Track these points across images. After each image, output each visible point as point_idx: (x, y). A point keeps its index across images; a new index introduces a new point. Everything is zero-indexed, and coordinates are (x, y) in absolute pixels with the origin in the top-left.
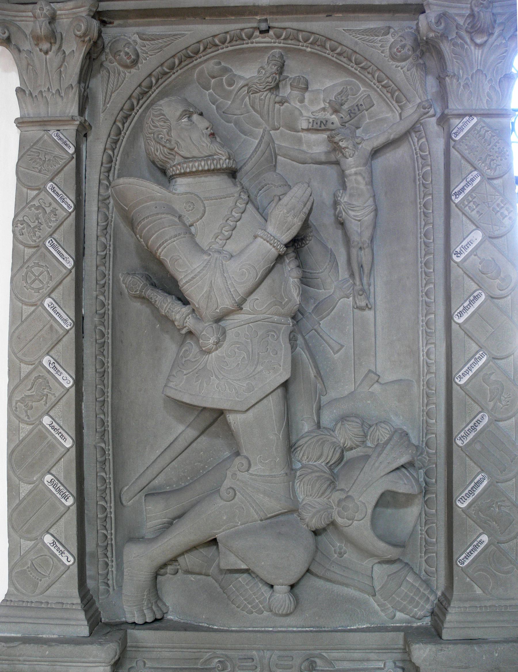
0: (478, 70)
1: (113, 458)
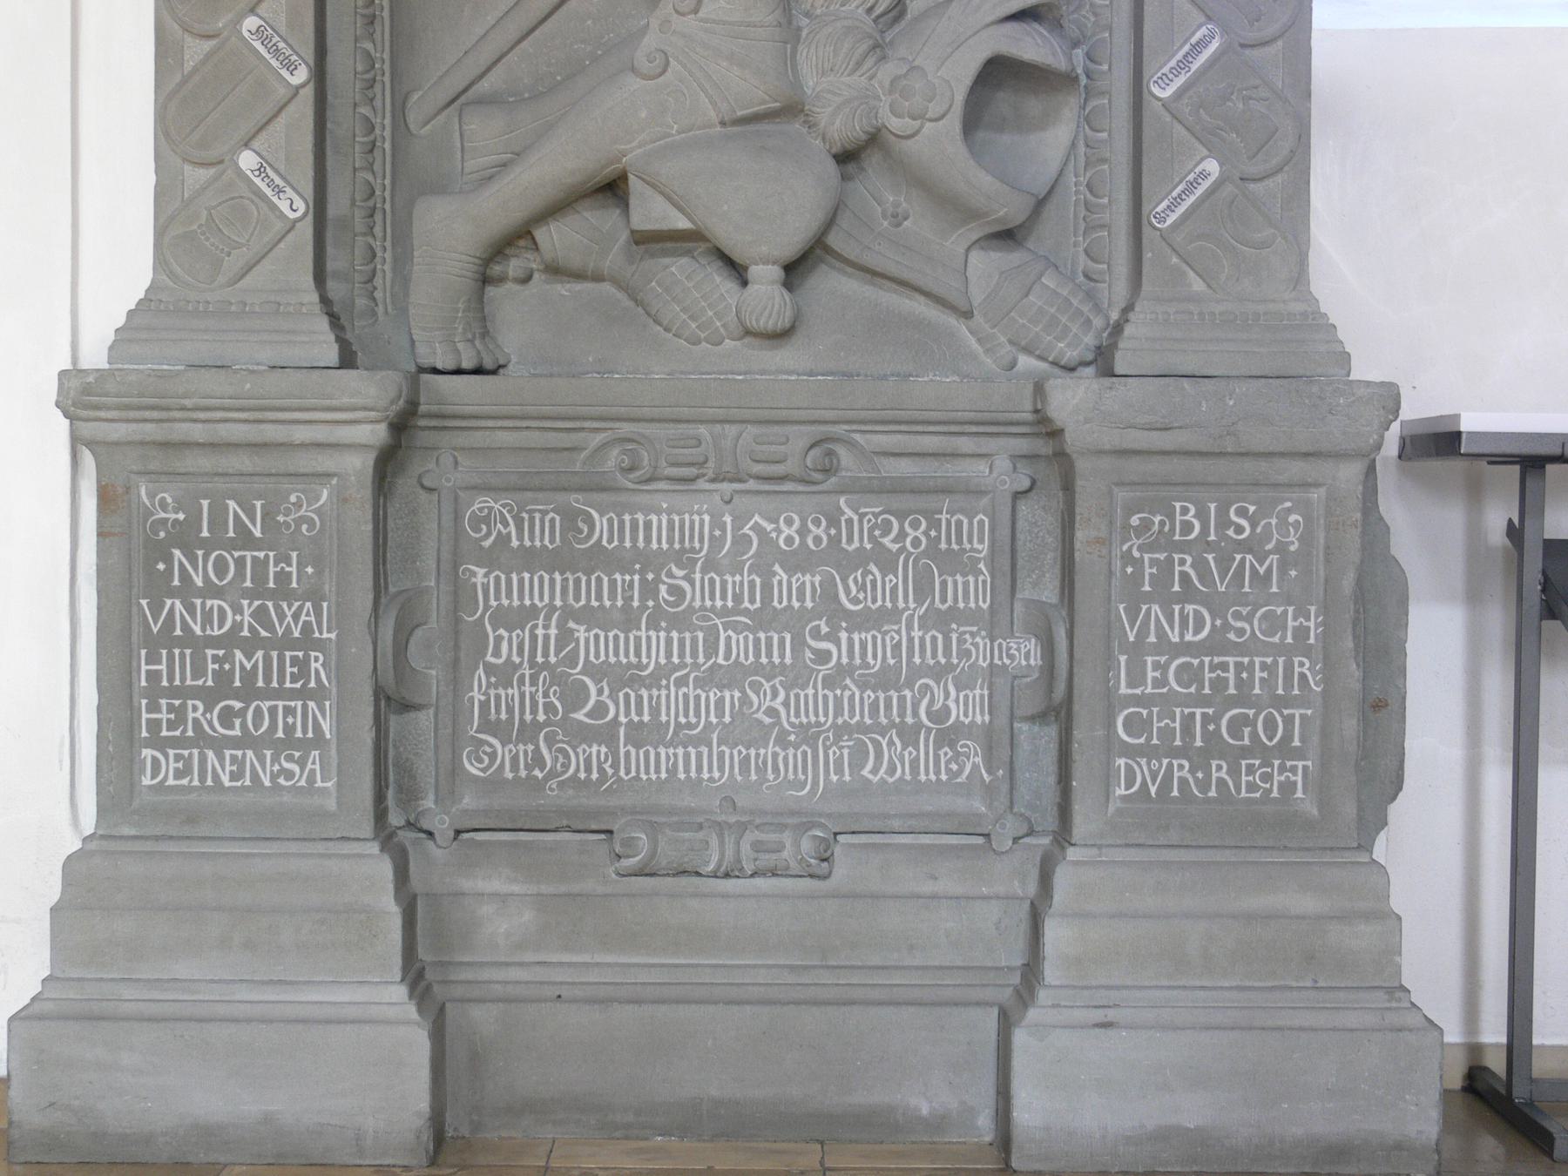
1: (392, 16)
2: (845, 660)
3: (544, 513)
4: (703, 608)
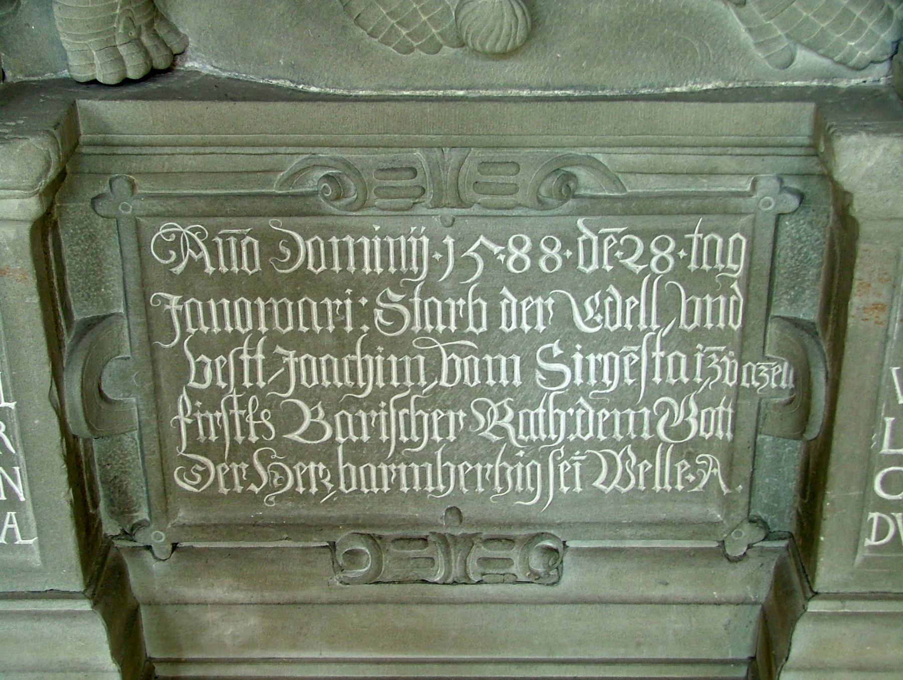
2: (579, 381)
3: (240, 237)
4: (423, 332)
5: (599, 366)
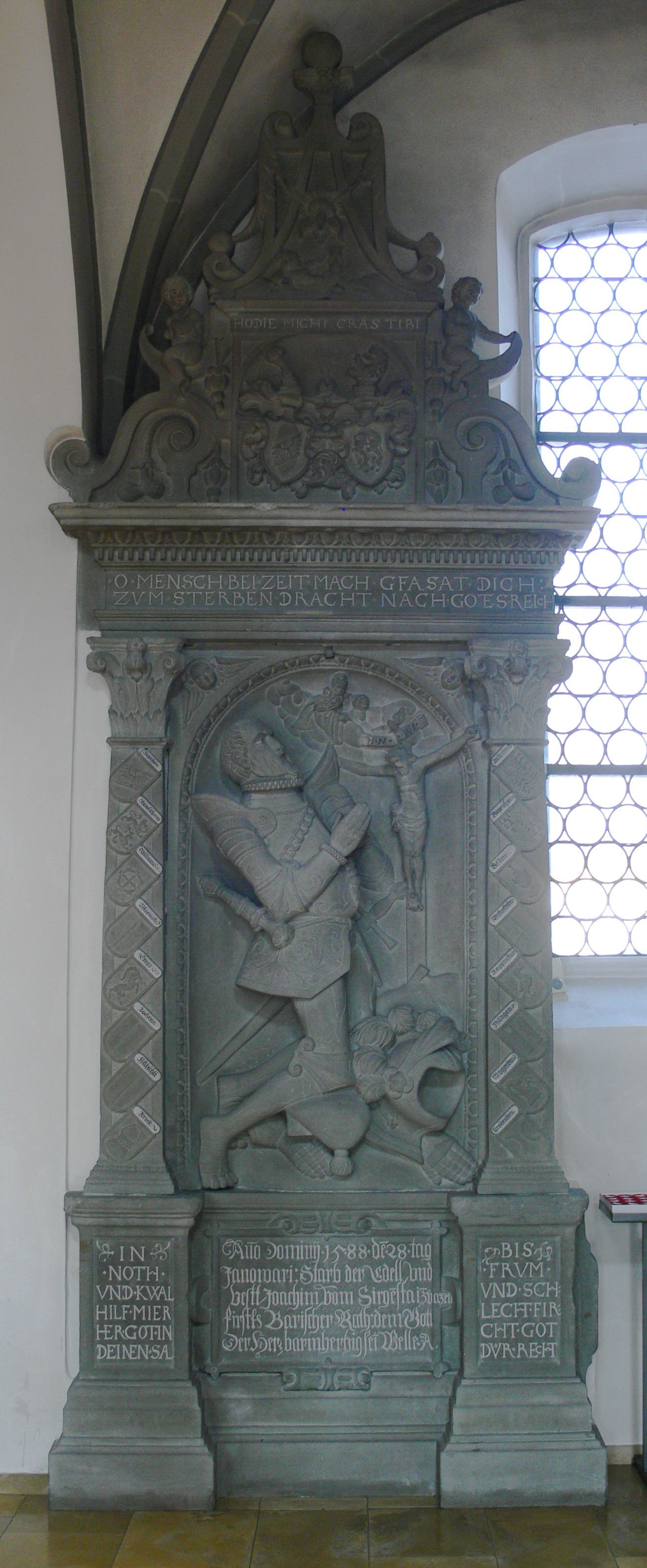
0: (516, 705)
2: (374, 1302)
3: (254, 1245)
4: (318, 1283)
5: (382, 1296)
